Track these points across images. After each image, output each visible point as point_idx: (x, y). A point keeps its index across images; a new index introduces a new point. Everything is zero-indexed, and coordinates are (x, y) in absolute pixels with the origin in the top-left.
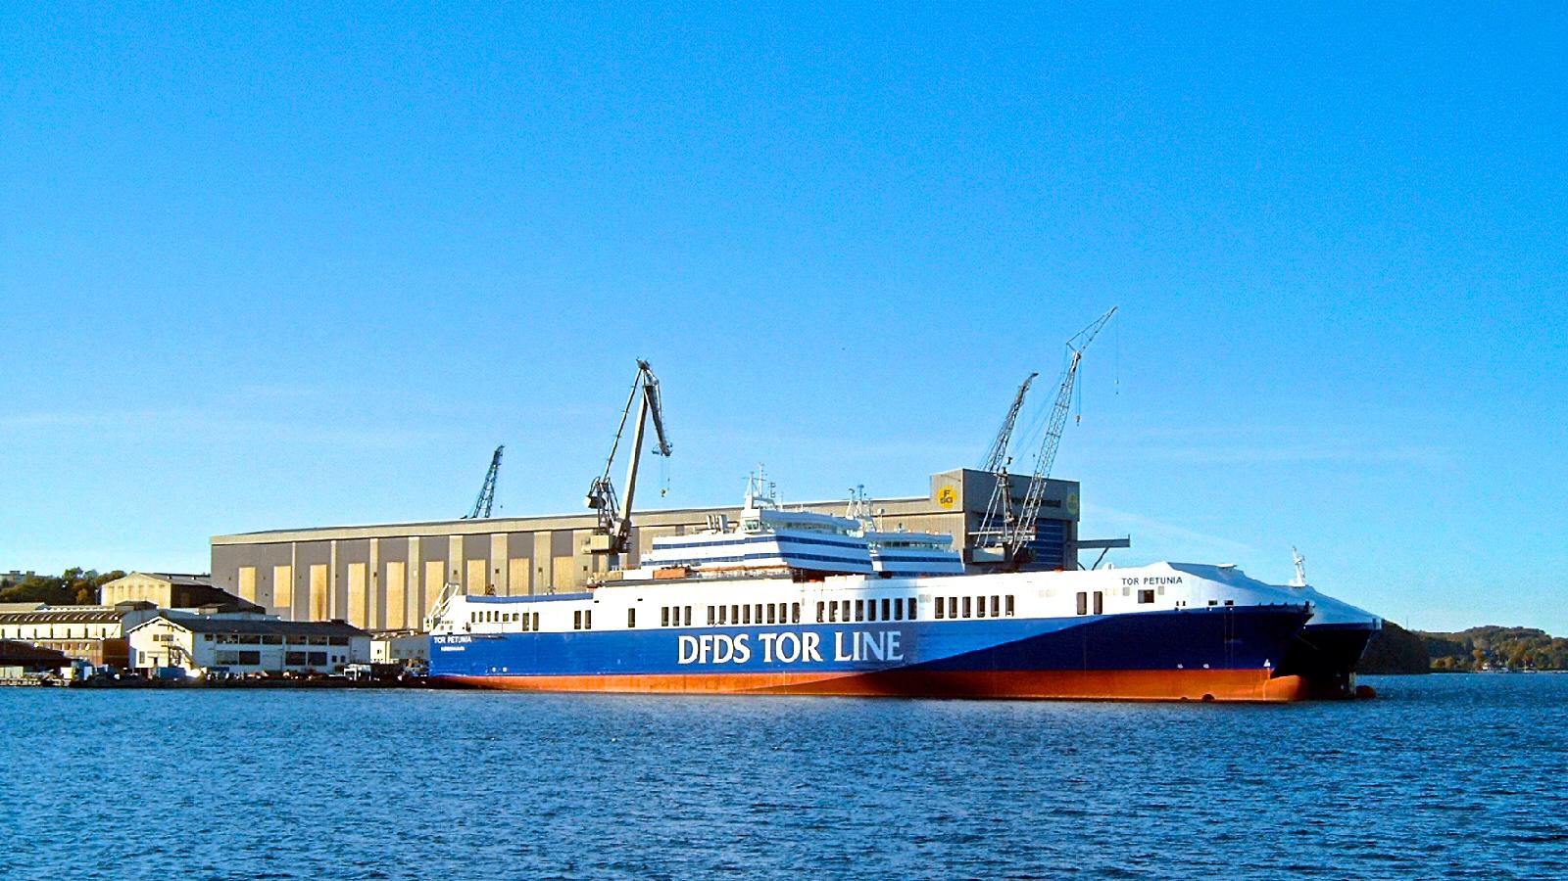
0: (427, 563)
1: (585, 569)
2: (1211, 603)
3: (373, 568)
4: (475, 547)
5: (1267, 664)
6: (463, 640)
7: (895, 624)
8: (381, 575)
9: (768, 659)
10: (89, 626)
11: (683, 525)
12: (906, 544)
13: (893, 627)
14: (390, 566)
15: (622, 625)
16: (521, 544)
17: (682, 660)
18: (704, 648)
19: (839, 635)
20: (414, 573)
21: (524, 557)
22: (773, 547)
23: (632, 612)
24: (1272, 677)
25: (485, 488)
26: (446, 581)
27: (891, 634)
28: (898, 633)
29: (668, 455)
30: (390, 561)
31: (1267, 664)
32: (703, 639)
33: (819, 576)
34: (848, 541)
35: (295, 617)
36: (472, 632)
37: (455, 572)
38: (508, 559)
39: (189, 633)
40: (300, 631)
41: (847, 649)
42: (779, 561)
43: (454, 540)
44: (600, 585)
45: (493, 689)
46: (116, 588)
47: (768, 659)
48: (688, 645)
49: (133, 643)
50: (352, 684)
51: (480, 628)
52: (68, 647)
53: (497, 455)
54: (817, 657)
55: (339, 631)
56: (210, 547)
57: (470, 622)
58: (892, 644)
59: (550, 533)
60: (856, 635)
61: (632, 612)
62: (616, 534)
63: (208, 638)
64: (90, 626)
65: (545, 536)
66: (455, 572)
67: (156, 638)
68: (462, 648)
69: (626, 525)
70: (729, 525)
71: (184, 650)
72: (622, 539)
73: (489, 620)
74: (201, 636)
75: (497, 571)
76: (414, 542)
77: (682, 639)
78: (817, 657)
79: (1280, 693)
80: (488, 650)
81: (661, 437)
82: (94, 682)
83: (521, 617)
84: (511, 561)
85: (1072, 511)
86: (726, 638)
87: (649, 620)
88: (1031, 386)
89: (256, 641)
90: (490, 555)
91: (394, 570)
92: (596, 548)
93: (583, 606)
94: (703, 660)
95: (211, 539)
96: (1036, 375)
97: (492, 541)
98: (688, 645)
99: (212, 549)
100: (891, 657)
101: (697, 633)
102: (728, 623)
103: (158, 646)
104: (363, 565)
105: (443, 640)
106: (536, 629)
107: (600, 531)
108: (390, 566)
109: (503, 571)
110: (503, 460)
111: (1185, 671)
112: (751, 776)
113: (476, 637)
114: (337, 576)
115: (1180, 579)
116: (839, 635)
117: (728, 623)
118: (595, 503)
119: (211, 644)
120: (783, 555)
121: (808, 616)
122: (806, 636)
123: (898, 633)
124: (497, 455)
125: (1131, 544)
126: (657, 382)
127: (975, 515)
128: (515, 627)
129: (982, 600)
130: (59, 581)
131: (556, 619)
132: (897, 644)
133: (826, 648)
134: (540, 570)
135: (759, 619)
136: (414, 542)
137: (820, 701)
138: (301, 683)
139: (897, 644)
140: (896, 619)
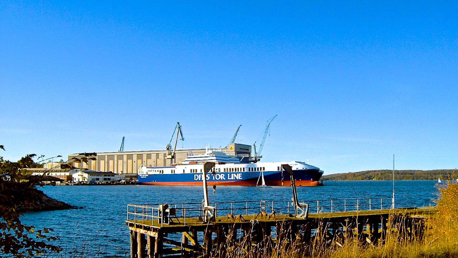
0: (101, 161)
1: (154, 161)
2: (303, 168)
3: (106, 161)
4: (120, 157)
5: (312, 179)
6: (146, 175)
7: (251, 172)
8: (108, 163)
9: (214, 179)
10: (52, 173)
11: (133, 154)
12: (231, 157)
13: (240, 173)
14: (110, 161)
15: (182, 173)
16: (130, 157)
17: (195, 179)
18: (200, 177)
19: (229, 174)
20: (116, 162)
21: (121, 160)
22: (215, 158)
23: (184, 170)
24: (312, 182)
25: (121, 145)
26: (142, 164)
27: (240, 174)
28: (241, 174)
29: (183, 140)
30: (110, 160)
31: (312, 179)
32: (200, 175)
33: (224, 163)
34: (225, 157)
35: (98, 170)
36: (148, 174)
37: (125, 162)
38: (147, 159)
39: (87, 174)
40: (105, 174)
41: (230, 177)
42: (216, 161)
43: (134, 156)
44: (177, 165)
45: (152, 185)
46: (47, 165)
47: (214, 179)
48: (196, 176)
49: (73, 176)
50: (122, 184)
51: (149, 173)
52: (60, 177)
53: (123, 138)
54: (224, 179)
55: (112, 174)
56: (68, 157)
57: (147, 172)
58: (240, 176)
59: (156, 154)
60: (232, 174)
61: (184, 170)
62: (173, 155)
63: (91, 175)
64: (66, 173)
65: (145, 155)
66: (125, 162)
67: (79, 175)
68: (146, 177)
69: (174, 154)
70: (193, 153)
71: (86, 178)
72: (173, 156)
73: (241, 168)
74: (89, 175)
75: (135, 162)
76: (116, 156)
77: (195, 175)
78: (224, 179)
79: (315, 184)
80: (151, 178)
81: (182, 137)
82: (78, 184)
83: (159, 171)
84: (138, 160)
85: (250, 151)
86: (197, 175)
87: (188, 171)
88: (240, 127)
89: (110, 176)
90: (123, 158)
91: (111, 162)
92: (168, 158)
93: (173, 169)
94: (200, 179)
95: (68, 155)
96: (241, 125)
97: (143, 156)
98: (196, 176)
99: (68, 158)
100: (240, 178)
101: (198, 174)
102: (234, 171)
103: (80, 177)
104: (122, 160)
105: (141, 176)
106: (174, 173)
107: (169, 155)
108: (110, 161)
109: (146, 162)
110: (124, 139)
111: (297, 181)
112: (83, 212)
113: (149, 175)
114: (98, 163)
115: (297, 164)
116: (229, 174)
117: (234, 171)
118: (168, 149)
119: (91, 176)
120: (216, 159)
121: (222, 171)
122: (222, 175)
123: (241, 174)
124: (123, 138)
125: (262, 157)
126: (181, 126)
127: (237, 153)
128: (158, 173)
129: (238, 169)
130: (17, 163)
131: (167, 171)
132: (241, 176)
133: (226, 177)
134: (144, 162)
135: (227, 171)
136: (116, 156)
137: (225, 186)
138: (107, 184)
139: (241, 176)
140: (243, 171)
